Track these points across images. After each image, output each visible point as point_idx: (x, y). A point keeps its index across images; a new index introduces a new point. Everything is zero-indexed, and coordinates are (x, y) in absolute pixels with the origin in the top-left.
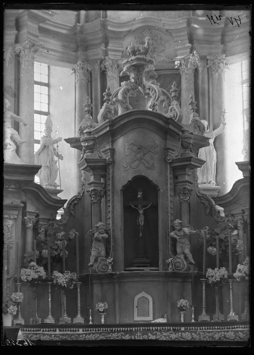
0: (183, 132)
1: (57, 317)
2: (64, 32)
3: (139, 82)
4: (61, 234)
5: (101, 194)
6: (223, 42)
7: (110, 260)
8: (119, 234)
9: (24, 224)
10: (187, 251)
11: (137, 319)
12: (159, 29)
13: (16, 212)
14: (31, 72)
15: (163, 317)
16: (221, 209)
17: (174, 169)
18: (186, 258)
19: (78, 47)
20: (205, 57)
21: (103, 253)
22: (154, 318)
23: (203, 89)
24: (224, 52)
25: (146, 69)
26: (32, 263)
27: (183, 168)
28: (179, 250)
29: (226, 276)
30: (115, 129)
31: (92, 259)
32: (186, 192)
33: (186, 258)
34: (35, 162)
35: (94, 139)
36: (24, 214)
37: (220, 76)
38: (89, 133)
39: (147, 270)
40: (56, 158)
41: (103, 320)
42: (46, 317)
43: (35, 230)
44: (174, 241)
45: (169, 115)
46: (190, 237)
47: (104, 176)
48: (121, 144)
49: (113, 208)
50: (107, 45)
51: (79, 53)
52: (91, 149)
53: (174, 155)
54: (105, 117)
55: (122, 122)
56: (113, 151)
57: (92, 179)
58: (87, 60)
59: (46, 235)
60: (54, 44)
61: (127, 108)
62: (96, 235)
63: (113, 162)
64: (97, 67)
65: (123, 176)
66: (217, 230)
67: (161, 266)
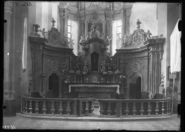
0: (104, 42)
1: (77, 81)
2: (75, 13)
3: (95, 31)
4: (78, 64)
5: (86, 55)
6: (113, 17)
7: (88, 69)
8: (90, 64)
9: (70, 61)
10: (104, 68)
11: (93, 82)
12: (98, 13)
13: (68, 59)
14: (67, 23)
15: (99, 82)
16: (112, 59)
17: (102, 50)
18: (104, 70)
19: (78, 17)
20: (109, 21)
21: (87, 68)
22: (97, 82)
23: (108, 29)
24: (113, 20)
25: (97, 28)
26: (72, 70)
27: (104, 50)
28: (102, 68)
29: (27, 111)
30: (90, 41)
31: (84, 69)
32: (104, 55)
33: (104, 70)
34: (7, 11)
35: (85, 43)
36: (70, 59)
37: (112, 25)
38: (84, 42)
39: (95, 72)
40: (73, 44)
41: (87, 82)
42: (74, 81)
43: (72, 63)
44: (101, 65)
45: (101, 39)
46: (105, 65)
47: (87, 52)
48: (91, 45)
49: (89, 58)
50: (85, 17)
51: (78, 19)
52: (84, 45)
53: (102, 47)
54: (88, 38)
55: (92, 40)
56: (89, 46)
57: (84, 52)
58: (80, 21)
59: (74, 64)
60: (72, 16)
61: (92, 37)
62: (85, 64)
63: (89, 49)
64: (83, 22)
65: (91, 51)
66: (111, 64)
67: (99, 71)
